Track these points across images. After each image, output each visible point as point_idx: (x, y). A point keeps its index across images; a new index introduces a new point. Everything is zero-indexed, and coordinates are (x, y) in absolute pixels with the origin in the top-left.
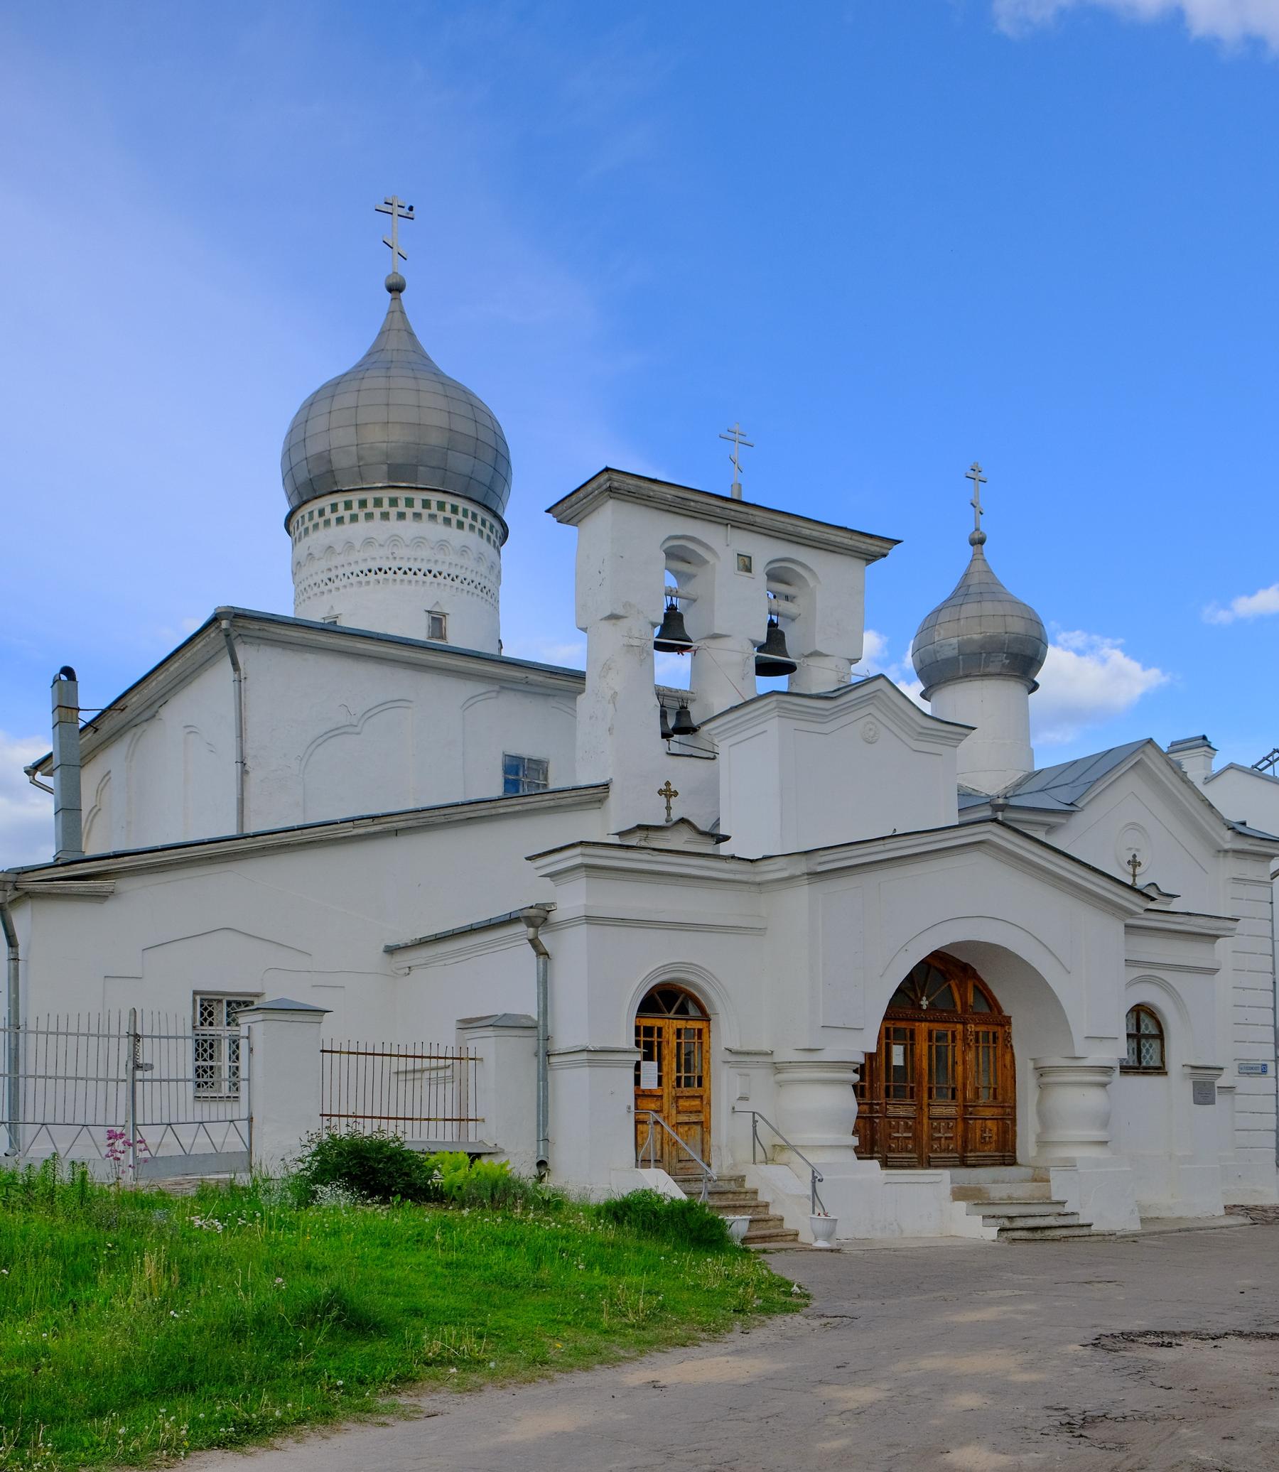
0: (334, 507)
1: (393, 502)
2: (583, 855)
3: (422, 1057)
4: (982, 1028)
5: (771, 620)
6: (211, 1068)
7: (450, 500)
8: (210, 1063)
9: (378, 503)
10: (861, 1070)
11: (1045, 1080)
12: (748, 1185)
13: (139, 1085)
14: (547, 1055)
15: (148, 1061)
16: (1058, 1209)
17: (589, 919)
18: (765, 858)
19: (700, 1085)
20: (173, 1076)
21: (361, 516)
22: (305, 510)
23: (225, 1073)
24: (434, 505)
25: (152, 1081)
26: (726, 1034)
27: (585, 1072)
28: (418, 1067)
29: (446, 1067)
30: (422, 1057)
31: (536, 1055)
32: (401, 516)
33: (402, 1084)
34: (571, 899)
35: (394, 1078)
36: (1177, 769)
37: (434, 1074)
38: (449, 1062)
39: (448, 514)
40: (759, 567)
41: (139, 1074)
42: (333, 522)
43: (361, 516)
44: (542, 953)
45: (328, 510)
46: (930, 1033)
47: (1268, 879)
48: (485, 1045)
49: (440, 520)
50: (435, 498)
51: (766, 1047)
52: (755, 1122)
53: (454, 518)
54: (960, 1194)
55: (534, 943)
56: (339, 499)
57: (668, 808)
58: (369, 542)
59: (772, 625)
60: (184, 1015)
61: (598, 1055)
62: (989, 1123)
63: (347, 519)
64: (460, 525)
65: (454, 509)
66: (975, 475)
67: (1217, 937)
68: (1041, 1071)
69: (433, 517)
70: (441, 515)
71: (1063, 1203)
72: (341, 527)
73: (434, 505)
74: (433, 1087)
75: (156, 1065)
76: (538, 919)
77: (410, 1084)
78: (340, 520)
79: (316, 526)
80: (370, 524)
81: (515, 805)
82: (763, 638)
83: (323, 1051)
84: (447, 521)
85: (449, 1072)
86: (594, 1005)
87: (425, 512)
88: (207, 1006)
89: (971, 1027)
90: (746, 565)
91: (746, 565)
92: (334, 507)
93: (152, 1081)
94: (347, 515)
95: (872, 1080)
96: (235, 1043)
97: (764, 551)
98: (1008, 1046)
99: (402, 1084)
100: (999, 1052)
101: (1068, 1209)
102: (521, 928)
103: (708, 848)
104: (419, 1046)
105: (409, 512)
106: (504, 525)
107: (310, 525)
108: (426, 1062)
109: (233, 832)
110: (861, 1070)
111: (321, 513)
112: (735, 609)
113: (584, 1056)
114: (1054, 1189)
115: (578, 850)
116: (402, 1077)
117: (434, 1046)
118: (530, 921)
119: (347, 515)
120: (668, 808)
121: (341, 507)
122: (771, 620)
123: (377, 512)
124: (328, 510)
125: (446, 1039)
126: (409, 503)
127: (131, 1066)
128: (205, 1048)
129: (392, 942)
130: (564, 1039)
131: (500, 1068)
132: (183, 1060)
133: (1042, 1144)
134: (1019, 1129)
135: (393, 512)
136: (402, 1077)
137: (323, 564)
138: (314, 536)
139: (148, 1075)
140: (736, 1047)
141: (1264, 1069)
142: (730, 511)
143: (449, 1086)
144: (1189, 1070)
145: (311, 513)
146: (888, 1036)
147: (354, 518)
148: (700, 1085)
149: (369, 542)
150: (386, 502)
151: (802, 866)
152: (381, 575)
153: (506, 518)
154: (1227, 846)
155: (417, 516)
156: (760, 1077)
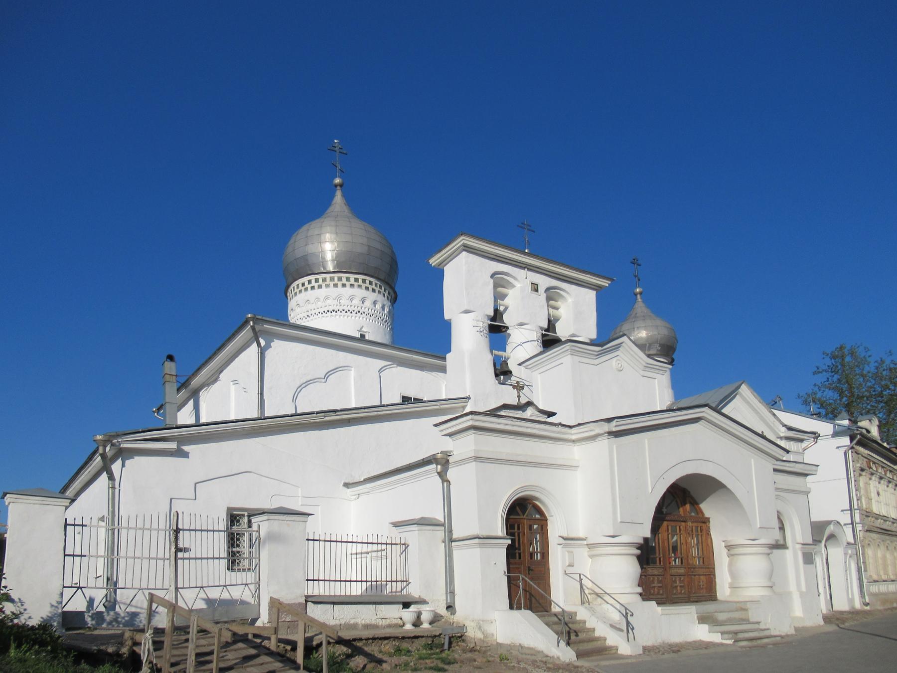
0: (310, 282)
1: (340, 279)
2: (472, 420)
3: (372, 543)
4: (695, 524)
6: (238, 552)
7: (368, 278)
8: (238, 549)
9: (332, 279)
10: (640, 547)
11: (732, 552)
12: (578, 618)
13: (180, 562)
15: (187, 545)
16: (756, 626)
17: (477, 459)
18: (580, 424)
19: (520, 558)
20: (205, 556)
21: (324, 285)
23: (247, 555)
24: (360, 280)
25: (190, 559)
27: (477, 551)
28: (369, 549)
29: (382, 550)
30: (372, 543)
31: (444, 542)
32: (344, 285)
33: (354, 561)
35: (349, 557)
37: (374, 554)
38: (384, 546)
39: (367, 285)
40: (542, 290)
41: (180, 555)
42: (309, 289)
43: (324, 285)
45: (306, 283)
47: (801, 451)
48: (412, 535)
49: (364, 287)
50: (361, 277)
51: (581, 535)
52: (581, 580)
53: (370, 287)
54: (702, 620)
56: (312, 277)
57: (519, 397)
58: (327, 298)
59: (549, 321)
61: (485, 539)
62: (702, 577)
63: (316, 287)
64: (374, 291)
65: (371, 283)
66: (635, 262)
67: (806, 475)
68: (729, 547)
69: (360, 286)
70: (364, 285)
71: (758, 623)
72: (313, 291)
73: (360, 280)
74: (379, 562)
75: (193, 548)
76: (441, 462)
77: (359, 560)
78: (313, 288)
79: (300, 291)
80: (328, 289)
82: (546, 326)
83: (308, 540)
84: (367, 288)
85: (384, 553)
86: (480, 510)
87: (356, 284)
88: (233, 518)
89: (689, 524)
90: (535, 288)
92: (310, 282)
93: (190, 559)
94: (316, 285)
95: (646, 554)
96: (520, 554)
98: (709, 534)
99: (354, 561)
100: (704, 538)
101: (762, 626)
103: (544, 418)
104: (380, 537)
105: (348, 284)
106: (395, 293)
107: (298, 291)
108: (375, 547)
110: (640, 547)
111: (303, 285)
113: (477, 541)
114: (750, 614)
115: (470, 417)
116: (354, 556)
117: (380, 537)
119: (316, 285)
120: (519, 397)
121: (313, 281)
123: (332, 284)
124: (306, 283)
125: (388, 533)
126: (348, 279)
127: (173, 550)
128: (233, 540)
129: (347, 481)
131: (425, 548)
132: (219, 545)
133: (732, 587)
134: (718, 580)
135: (340, 284)
136: (354, 556)
137: (304, 309)
138: (299, 296)
139: (186, 555)
140: (565, 535)
143: (384, 561)
144: (800, 546)
145: (298, 285)
146: (655, 529)
147: (320, 287)
148: (520, 558)
149: (327, 298)
150: (336, 279)
151: (606, 427)
152: (334, 313)
153: (396, 289)
154: (782, 435)
155: (352, 286)
156: (582, 553)
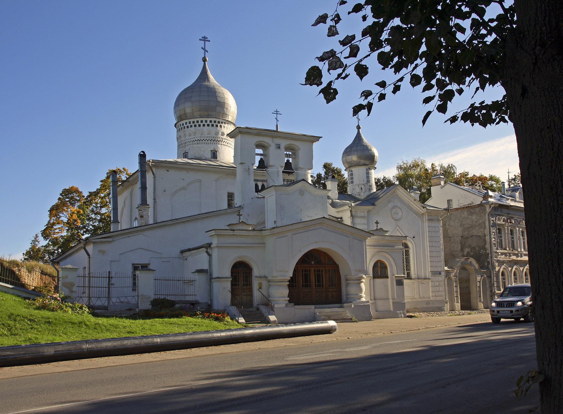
0: (186, 123)
5: (288, 161)
14: (211, 278)
17: (217, 247)
22: (179, 123)
26: (256, 272)
34: (215, 242)
36: (35, 293)
40: (282, 147)
44: (209, 255)
46: (315, 270)
55: (207, 252)
56: (187, 121)
60: (130, 269)
76: (209, 246)
81: (230, 211)
88: (136, 268)
90: (279, 147)
91: (279, 147)
92: (190, 123)
94: (188, 124)
95: (292, 283)
97: (284, 143)
102: (204, 249)
109: (129, 227)
110: (289, 281)
112: (278, 160)
118: (206, 248)
122: (288, 161)
130: (215, 275)
141: (440, 274)
142: (274, 134)
